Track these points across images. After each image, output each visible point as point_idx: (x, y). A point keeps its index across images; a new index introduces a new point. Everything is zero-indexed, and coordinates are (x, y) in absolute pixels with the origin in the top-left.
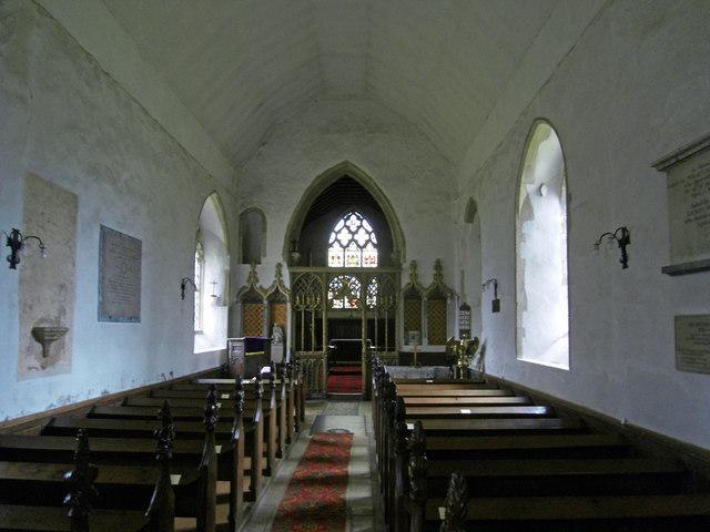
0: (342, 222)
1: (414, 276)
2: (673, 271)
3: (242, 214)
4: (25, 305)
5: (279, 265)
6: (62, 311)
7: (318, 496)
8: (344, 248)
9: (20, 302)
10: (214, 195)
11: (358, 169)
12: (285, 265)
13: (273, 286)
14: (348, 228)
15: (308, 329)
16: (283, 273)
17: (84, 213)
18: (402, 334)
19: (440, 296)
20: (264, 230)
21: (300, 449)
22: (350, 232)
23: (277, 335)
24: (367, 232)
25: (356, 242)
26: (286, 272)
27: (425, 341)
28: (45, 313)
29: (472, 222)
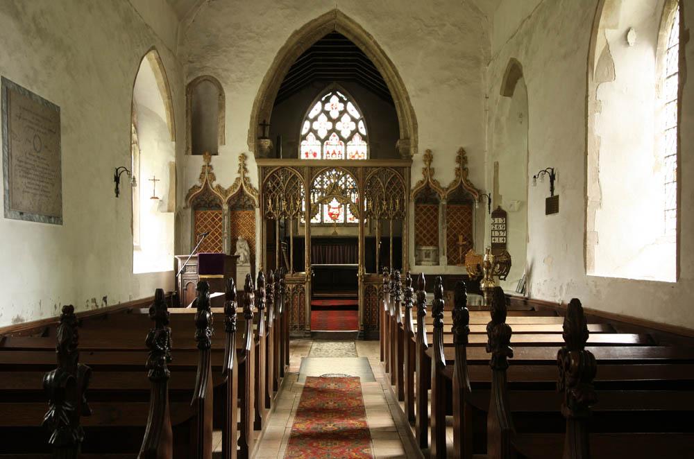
0: (318, 106)
1: (429, 171)
3: (190, 85)
5: (243, 157)
8: (323, 141)
10: (152, 54)
12: (251, 156)
13: (235, 185)
14: (327, 113)
15: (284, 247)
16: (248, 167)
19: (464, 198)
20: (222, 107)
21: (293, 399)
22: (330, 119)
24: (353, 119)
25: (338, 133)
27: (443, 259)
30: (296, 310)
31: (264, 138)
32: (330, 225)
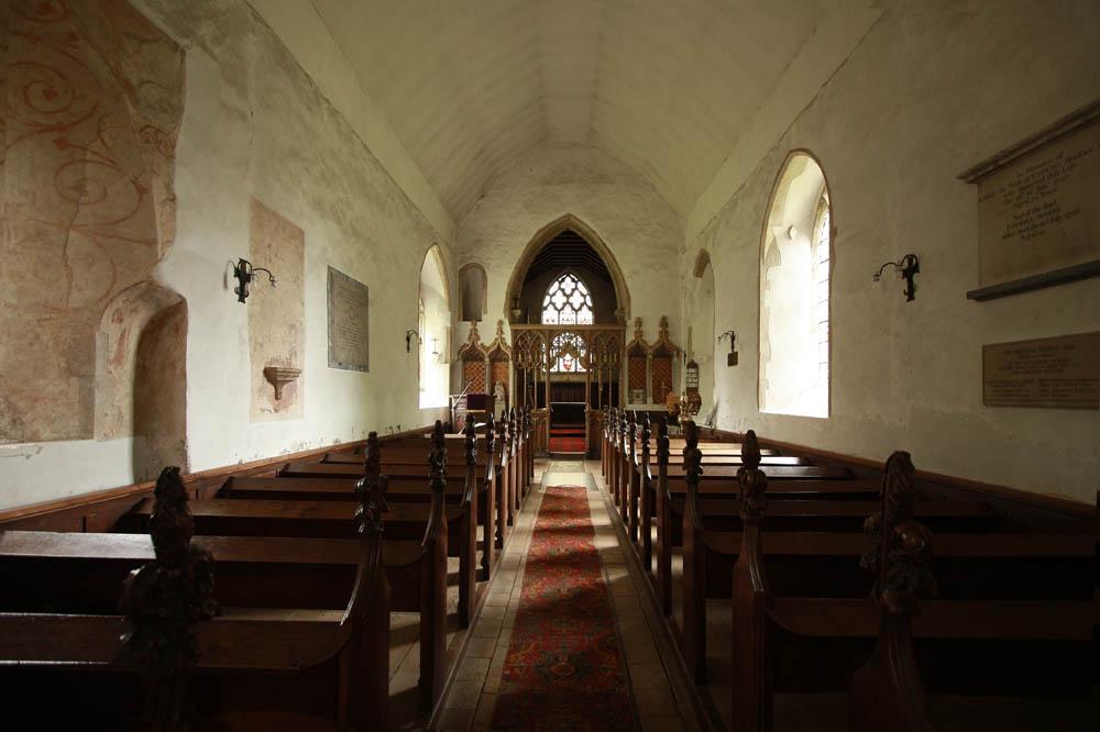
0: (556, 284)
1: (639, 334)
2: (981, 296)
4: (256, 343)
5: (501, 323)
6: (293, 353)
7: (566, 545)
9: (250, 340)
10: (435, 248)
11: (582, 222)
12: (506, 322)
14: (563, 290)
17: (311, 251)
18: (626, 391)
19: (666, 353)
20: (485, 286)
23: (499, 393)
24: (582, 295)
25: (571, 305)
26: (507, 329)
27: (650, 400)
28: (277, 354)
29: (701, 276)
30: (539, 437)
31: (515, 308)
32: (564, 373)
